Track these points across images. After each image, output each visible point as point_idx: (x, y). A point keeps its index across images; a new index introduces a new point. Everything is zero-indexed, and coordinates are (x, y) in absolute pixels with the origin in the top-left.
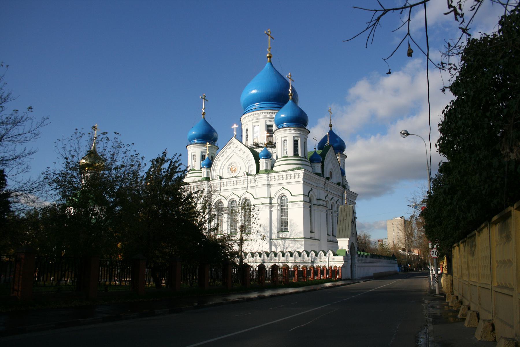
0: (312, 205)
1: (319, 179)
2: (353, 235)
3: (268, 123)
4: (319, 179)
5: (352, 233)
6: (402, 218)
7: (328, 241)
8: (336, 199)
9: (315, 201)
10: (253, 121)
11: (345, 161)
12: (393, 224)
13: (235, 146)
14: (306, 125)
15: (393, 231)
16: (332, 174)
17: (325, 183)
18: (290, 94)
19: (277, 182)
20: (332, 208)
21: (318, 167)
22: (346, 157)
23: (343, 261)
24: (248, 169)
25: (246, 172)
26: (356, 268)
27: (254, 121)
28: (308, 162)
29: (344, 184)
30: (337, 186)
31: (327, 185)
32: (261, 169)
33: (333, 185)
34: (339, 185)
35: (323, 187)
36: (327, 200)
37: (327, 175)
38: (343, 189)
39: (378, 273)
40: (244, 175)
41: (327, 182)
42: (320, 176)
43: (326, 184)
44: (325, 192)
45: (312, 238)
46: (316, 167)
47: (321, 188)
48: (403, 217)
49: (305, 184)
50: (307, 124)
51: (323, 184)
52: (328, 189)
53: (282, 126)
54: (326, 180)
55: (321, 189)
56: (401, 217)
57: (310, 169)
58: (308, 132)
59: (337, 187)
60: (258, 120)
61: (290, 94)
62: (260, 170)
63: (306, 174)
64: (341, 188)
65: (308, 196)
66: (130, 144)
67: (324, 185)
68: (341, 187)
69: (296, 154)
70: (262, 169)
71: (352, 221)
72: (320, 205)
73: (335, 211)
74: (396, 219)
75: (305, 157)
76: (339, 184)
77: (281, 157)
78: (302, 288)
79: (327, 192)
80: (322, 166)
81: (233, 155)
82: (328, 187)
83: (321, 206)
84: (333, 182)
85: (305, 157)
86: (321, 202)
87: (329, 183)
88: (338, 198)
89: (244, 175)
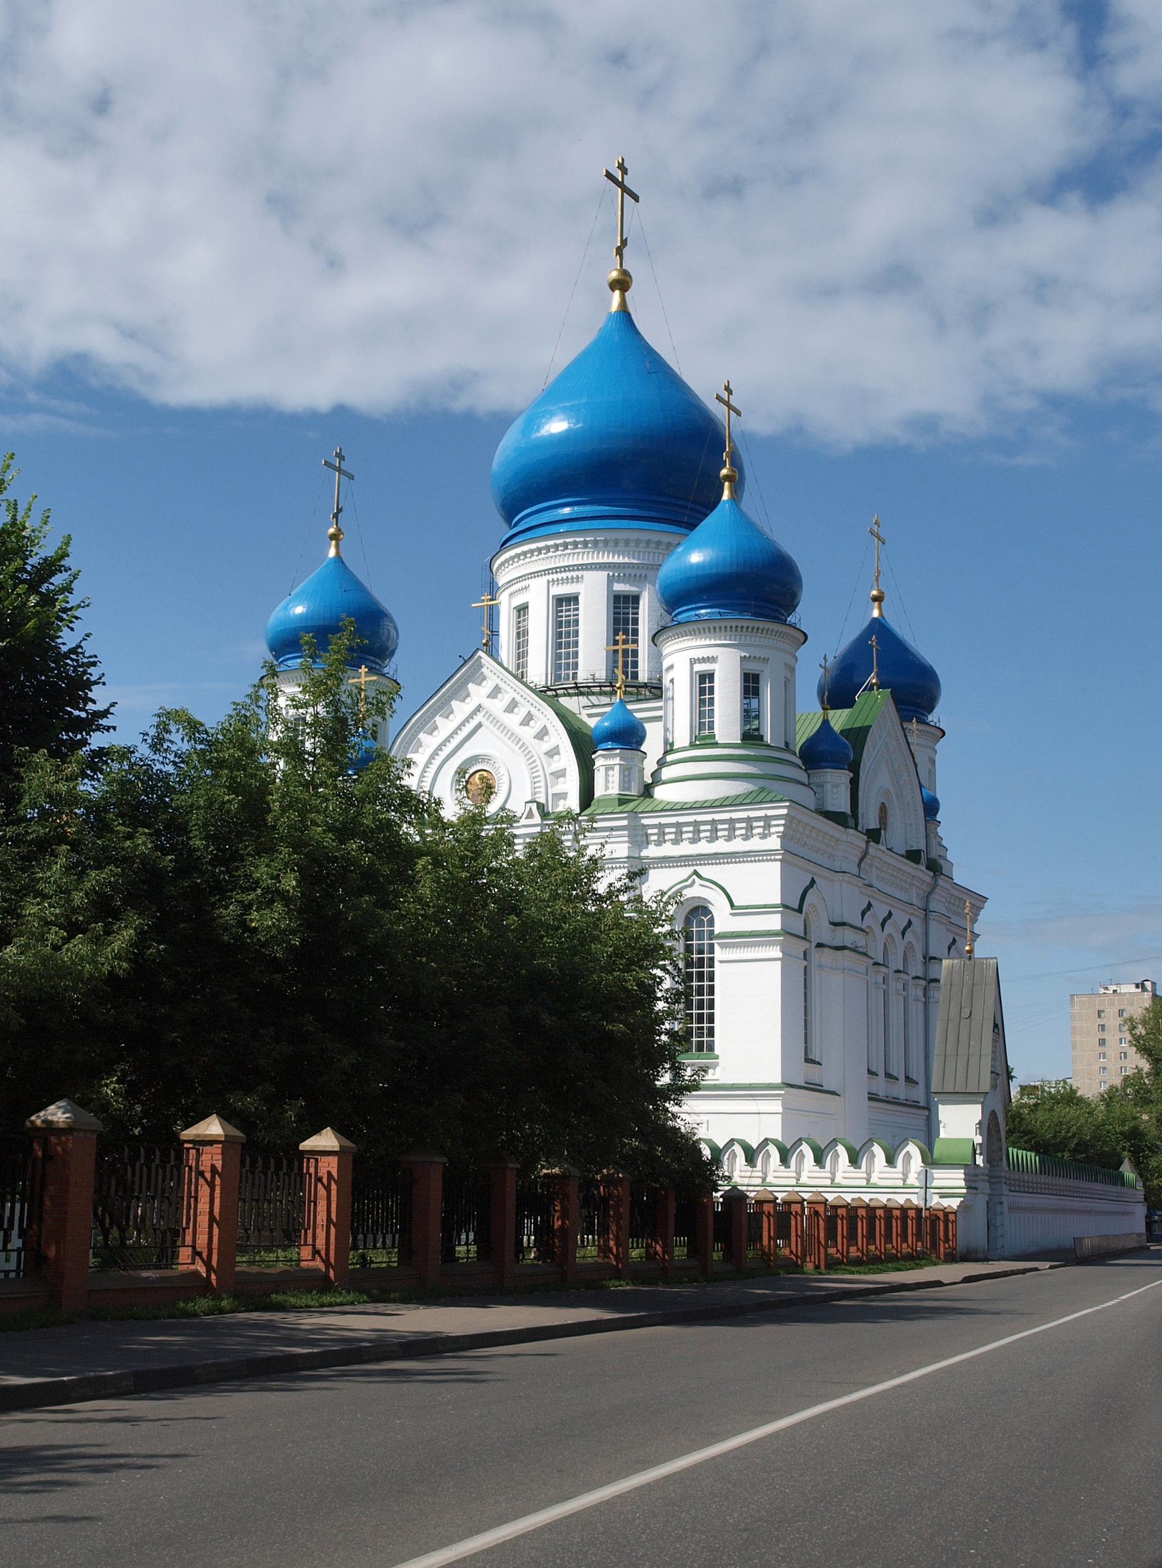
0: (814, 945)
1: (844, 837)
2: (996, 1080)
3: (619, 587)
4: (844, 837)
5: (992, 1072)
6: (1144, 989)
7: (870, 1099)
8: (900, 919)
9: (822, 932)
10: (550, 577)
11: (936, 752)
12: (1099, 1016)
13: (488, 686)
14: (791, 607)
15: (1101, 1049)
16: (886, 813)
17: (865, 854)
18: (724, 472)
19: (668, 850)
20: (805, 933)
21: (835, 786)
22: (944, 733)
23: (962, 1183)
24: (543, 790)
25: (538, 803)
26: (1002, 1213)
27: (555, 577)
28: (801, 768)
29: (933, 855)
30: (908, 867)
31: (869, 861)
32: (599, 792)
33: (893, 862)
34: (914, 862)
35: (855, 870)
36: (869, 927)
37: (870, 820)
38: (927, 876)
39: (730, 1325)
40: (530, 815)
41: (871, 850)
42: (845, 826)
43: (868, 860)
44: (861, 892)
45: (813, 1087)
46: (829, 787)
47: (847, 877)
48: (1148, 985)
49: (791, 864)
50: (795, 603)
51: (858, 861)
52: (874, 876)
53: (693, 613)
54: (867, 842)
55: (849, 882)
56: (1139, 981)
57: (806, 796)
58: (802, 638)
59: (910, 870)
60: (575, 574)
61: (724, 472)
62: (595, 797)
63: (793, 818)
64: (920, 872)
65: (800, 910)
66: (1100, 1035)
67: (861, 860)
68: (923, 868)
69: (751, 737)
70: (608, 792)
71: (996, 1026)
72: (843, 948)
73: (898, 971)
74: (1115, 991)
75: (787, 747)
76: (913, 856)
77: (687, 744)
78: (417, 1360)
79: (869, 891)
80: (851, 781)
81: (479, 726)
82: (874, 870)
83: (846, 952)
84: (890, 850)
85: (787, 744)
86: (847, 937)
87: (879, 854)
88: (891, 905)
89: (530, 815)
